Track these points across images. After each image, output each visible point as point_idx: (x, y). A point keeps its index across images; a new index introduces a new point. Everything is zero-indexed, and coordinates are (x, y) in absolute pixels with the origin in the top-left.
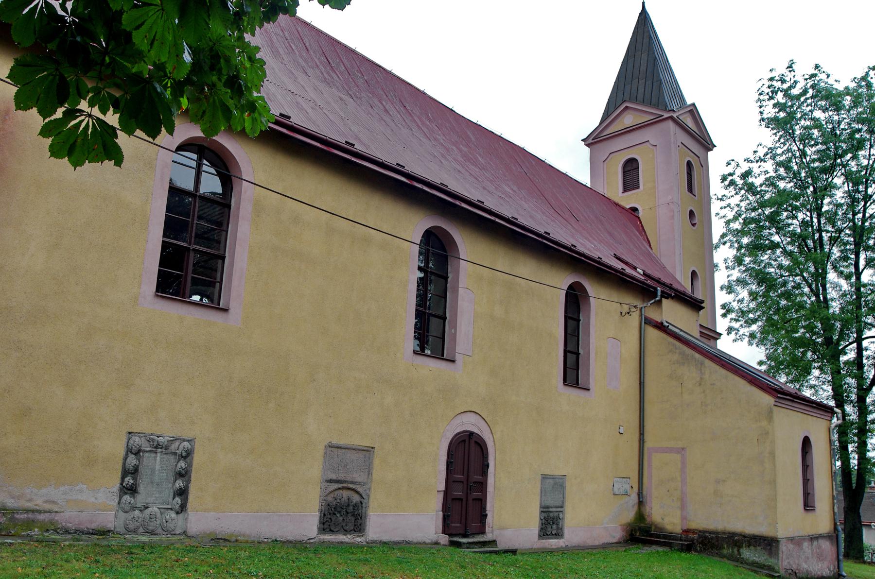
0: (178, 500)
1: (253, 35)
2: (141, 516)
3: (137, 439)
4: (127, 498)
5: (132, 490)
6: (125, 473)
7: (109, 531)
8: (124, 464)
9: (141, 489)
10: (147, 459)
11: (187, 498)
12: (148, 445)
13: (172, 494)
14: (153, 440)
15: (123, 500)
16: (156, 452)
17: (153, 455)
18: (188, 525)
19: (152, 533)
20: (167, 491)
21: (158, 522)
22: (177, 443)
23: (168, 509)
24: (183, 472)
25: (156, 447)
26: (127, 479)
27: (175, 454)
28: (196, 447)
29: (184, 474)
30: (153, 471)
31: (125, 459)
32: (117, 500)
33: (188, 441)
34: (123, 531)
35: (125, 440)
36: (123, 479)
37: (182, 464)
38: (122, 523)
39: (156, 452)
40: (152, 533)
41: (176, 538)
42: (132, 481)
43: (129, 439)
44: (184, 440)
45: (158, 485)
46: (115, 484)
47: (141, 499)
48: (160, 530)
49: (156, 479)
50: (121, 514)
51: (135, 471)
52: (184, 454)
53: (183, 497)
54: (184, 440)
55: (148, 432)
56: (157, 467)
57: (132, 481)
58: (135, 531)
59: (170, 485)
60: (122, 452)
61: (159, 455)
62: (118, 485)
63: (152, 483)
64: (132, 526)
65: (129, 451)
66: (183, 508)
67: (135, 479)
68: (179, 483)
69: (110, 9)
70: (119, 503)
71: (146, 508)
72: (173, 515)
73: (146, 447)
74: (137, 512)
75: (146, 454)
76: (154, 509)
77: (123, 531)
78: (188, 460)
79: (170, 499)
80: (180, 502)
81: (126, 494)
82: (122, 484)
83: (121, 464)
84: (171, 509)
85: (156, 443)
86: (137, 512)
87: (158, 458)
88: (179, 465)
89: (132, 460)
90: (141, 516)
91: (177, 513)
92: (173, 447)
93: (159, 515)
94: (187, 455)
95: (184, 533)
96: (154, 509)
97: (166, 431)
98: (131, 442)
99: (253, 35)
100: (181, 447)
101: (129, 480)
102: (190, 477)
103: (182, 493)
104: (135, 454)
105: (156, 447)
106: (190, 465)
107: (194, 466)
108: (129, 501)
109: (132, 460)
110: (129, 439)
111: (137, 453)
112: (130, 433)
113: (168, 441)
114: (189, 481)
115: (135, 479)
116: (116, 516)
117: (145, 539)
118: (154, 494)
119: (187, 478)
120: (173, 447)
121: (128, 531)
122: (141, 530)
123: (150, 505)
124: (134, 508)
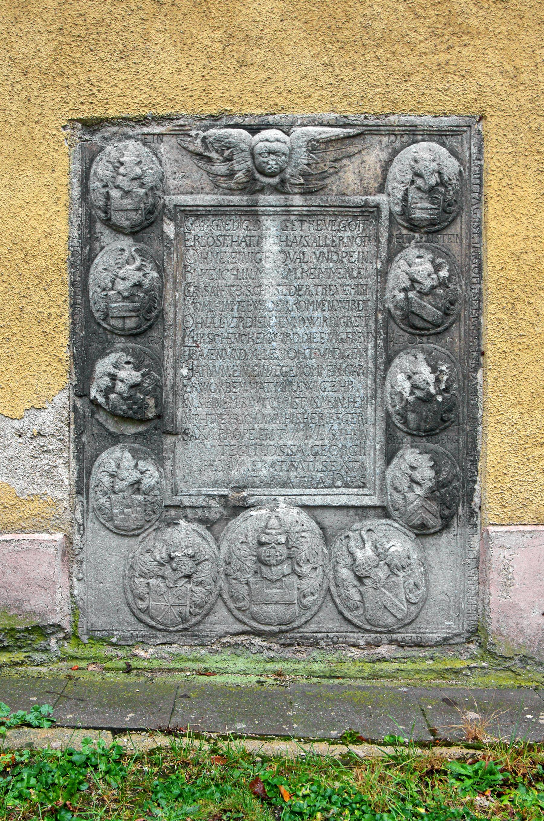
0: (415, 460)
1: (215, 774)
2: (207, 548)
3: (131, 151)
4: (118, 462)
5: (146, 420)
6: (90, 337)
7: (40, 630)
8: (80, 288)
9: (194, 409)
10: (207, 257)
11: (471, 452)
12: (197, 174)
13: (376, 434)
14: (227, 150)
15: (100, 476)
16: (251, 213)
17: (239, 229)
18: (494, 596)
19: (287, 636)
20: (347, 409)
21: (312, 581)
22: (373, 156)
23: (362, 510)
24: (429, 310)
25: (250, 187)
26: (104, 366)
27: (369, 212)
28: (495, 160)
29: (440, 321)
30: (249, 310)
31: (83, 260)
32: (67, 474)
33: (439, 135)
34: (124, 625)
35: (64, 161)
36: (83, 365)
37: (417, 264)
38: (111, 582)
39: (251, 213)
40: (287, 636)
41: (423, 663)
42: (129, 375)
43: (89, 158)
44: (413, 134)
45: (286, 384)
46: (46, 393)
47: (198, 464)
48: (328, 623)
49: (276, 356)
50: (104, 546)
51: (147, 318)
52: (422, 209)
53: (448, 443)
54: (413, 134)
55: (185, 105)
56: (269, 289)
57: (129, 375)
58: (189, 628)
59: (361, 386)
60: (56, 226)
61: (271, 227)
62: (63, 398)
63: (254, 379)
64: (165, 603)
65: (95, 218)
66: (451, 503)
67: (149, 362)
68: (413, 372)
69: (20, 709)
70: (82, 487)
71: (238, 508)
72: (399, 544)
73: (188, 186)
74: (185, 535)
75: (200, 230)
76: (281, 514)
77: (124, 625)
78: (453, 238)
79: (372, 460)
80: (426, 473)
81: (115, 439)
82: (81, 391)
83: (60, 290)
84: (384, 512)
85: (242, 166)
86: (185, 535)
87: (271, 246)
88: (399, 273)
89: (119, 265)
90: (207, 548)
91: (421, 531)
92: (354, 176)
93: (310, 543)
94: (445, 213)
95: (476, 633)
96: (281, 514)
97: (296, 93)
98: (101, 169)
99: (215, 774)
100: (400, 170)
101: (117, 369)
102: (476, 332)
103: (442, 421)
104: (136, 232)
105: (250, 187)
106: (472, 266)
107: (491, 273)
108: (129, 475)
109: (119, 265)
110: (89, 158)
111: (144, 226)
112: (91, 125)
113: (314, 146)
114: (474, 355)
115: (149, 362)
116: (70, 554)
117: (238, 670)
118: (277, 434)
119: (456, 338)
120: (354, 176)
121: (155, 628)
122: (221, 621)
123: (254, 495)
124: (163, 512)
